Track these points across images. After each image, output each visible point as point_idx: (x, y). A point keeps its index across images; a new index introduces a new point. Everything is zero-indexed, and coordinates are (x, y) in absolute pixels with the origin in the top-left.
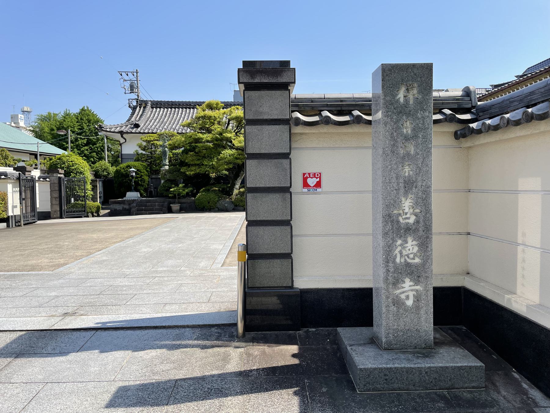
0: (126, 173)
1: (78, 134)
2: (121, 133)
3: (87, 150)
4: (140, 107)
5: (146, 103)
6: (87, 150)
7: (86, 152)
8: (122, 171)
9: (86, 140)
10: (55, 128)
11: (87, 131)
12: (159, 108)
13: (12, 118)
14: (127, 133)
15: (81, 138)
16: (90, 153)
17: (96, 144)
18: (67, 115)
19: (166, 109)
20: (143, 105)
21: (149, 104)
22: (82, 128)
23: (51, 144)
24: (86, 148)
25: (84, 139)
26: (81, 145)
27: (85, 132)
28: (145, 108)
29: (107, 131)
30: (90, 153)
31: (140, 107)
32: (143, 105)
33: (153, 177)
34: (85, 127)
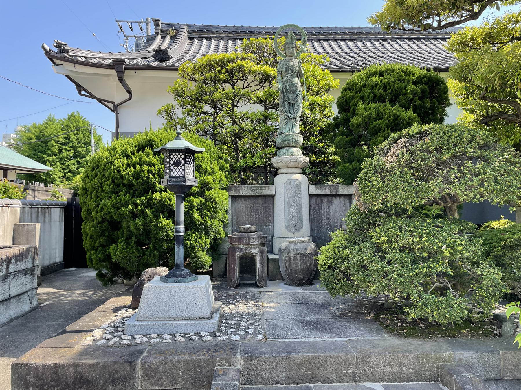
0: (137, 176)
1: (62, 144)
2: (119, 66)
3: (74, 164)
4: (163, 38)
5: (177, 28)
6: (74, 164)
7: (72, 167)
8: (120, 163)
9: (73, 151)
10: (33, 137)
11: (74, 140)
12: (207, 38)
13: (4, 137)
14: (136, 68)
15: (66, 149)
16: (77, 168)
17: (85, 157)
18: (51, 120)
19: (222, 43)
20: (171, 32)
21: (185, 30)
22: (68, 138)
23: (28, 156)
24: (73, 161)
25: (70, 150)
26: (67, 158)
27: (72, 142)
28: (173, 38)
29: (75, 62)
30: (77, 168)
31: (163, 38)
32: (171, 32)
33: (244, 191)
34: (72, 135)
